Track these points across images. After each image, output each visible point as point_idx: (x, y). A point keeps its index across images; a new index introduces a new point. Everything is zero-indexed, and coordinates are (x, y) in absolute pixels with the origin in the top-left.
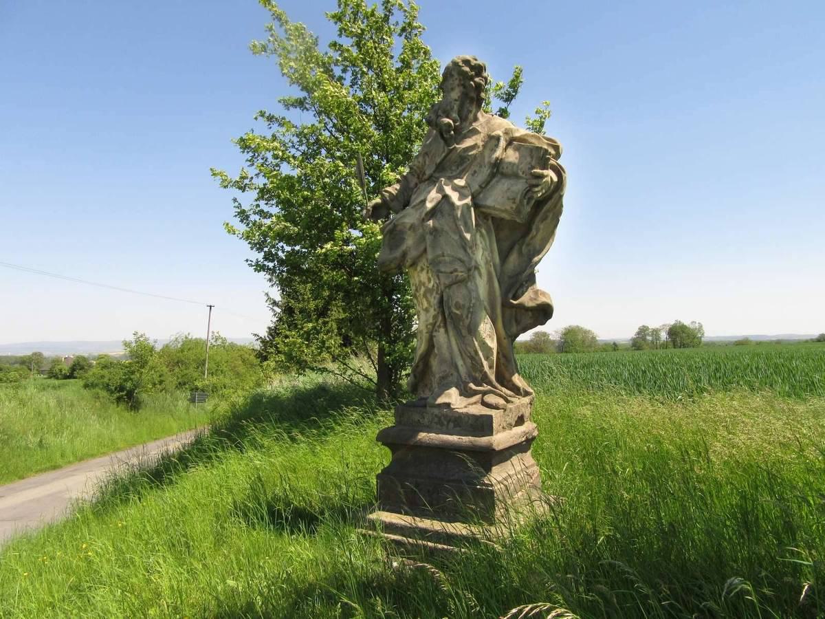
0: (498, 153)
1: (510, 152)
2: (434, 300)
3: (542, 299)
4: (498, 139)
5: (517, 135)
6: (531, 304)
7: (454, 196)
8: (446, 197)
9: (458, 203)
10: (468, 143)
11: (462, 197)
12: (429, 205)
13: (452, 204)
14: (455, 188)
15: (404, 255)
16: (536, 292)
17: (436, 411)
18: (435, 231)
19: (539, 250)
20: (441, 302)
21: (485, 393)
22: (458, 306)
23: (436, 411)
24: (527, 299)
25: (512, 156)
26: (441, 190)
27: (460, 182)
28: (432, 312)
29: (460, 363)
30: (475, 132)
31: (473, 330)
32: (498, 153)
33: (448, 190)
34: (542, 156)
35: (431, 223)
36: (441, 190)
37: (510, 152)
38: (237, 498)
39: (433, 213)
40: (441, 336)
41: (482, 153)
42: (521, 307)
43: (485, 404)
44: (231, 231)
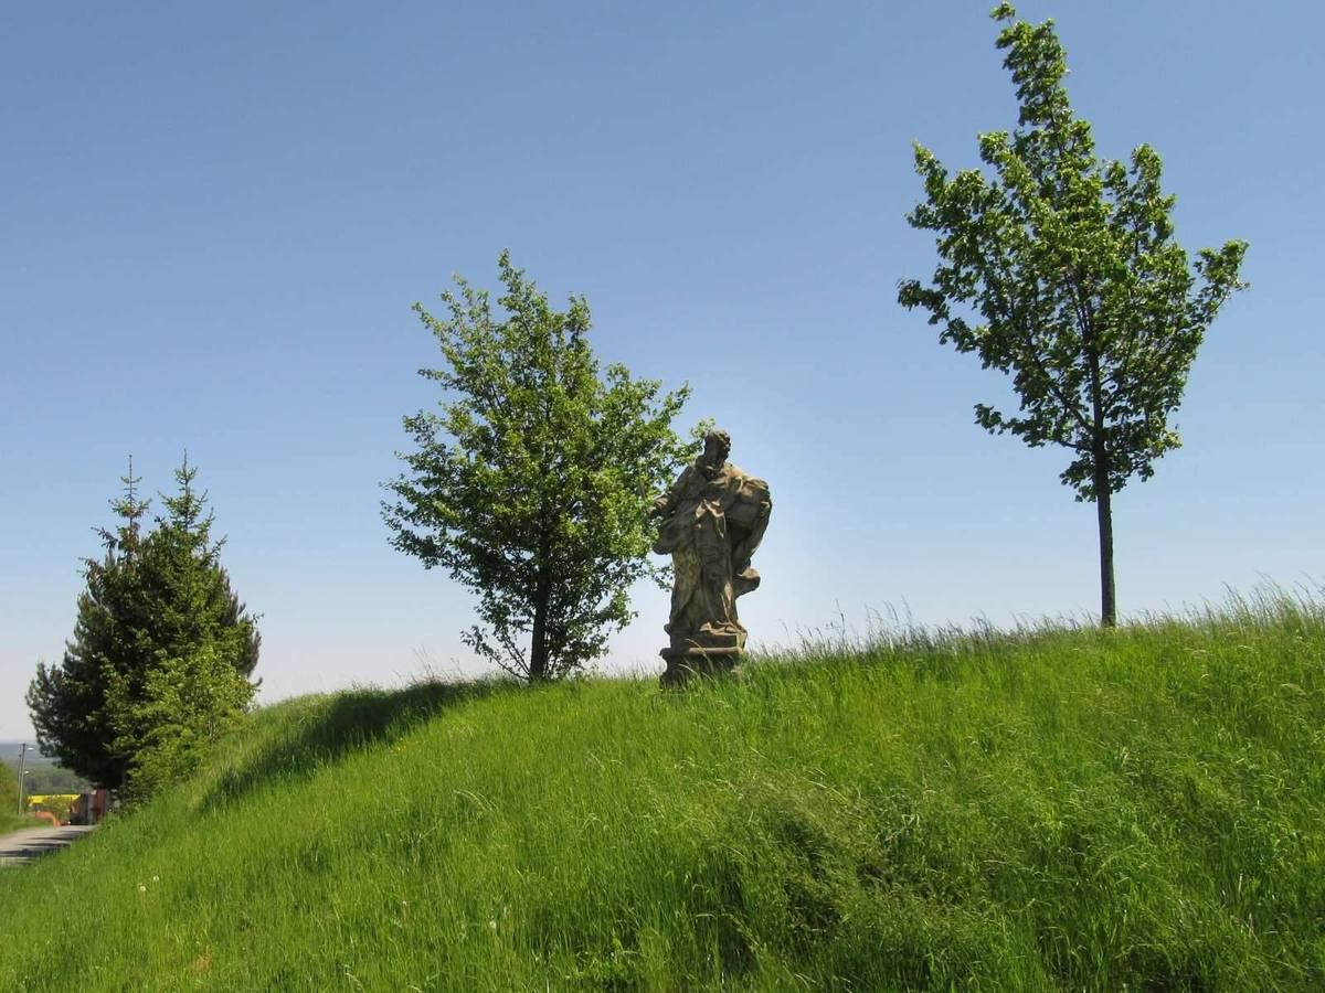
0: (740, 490)
1: (745, 489)
2: (698, 571)
3: (755, 575)
4: (739, 481)
5: (749, 479)
6: (749, 577)
7: (714, 512)
8: (708, 512)
9: (718, 516)
10: (720, 481)
11: (718, 512)
12: (698, 516)
13: (713, 517)
14: (713, 506)
15: (679, 543)
16: (752, 570)
17: (701, 636)
18: (701, 531)
19: (755, 545)
20: (702, 573)
21: (726, 626)
22: (714, 575)
23: (701, 636)
24: (746, 574)
25: (747, 492)
26: (704, 507)
27: (717, 503)
28: (696, 578)
29: (710, 609)
30: (724, 475)
31: (721, 589)
32: (740, 490)
33: (709, 507)
34: (762, 494)
35: (699, 526)
36: (704, 507)
37: (745, 489)
38: (354, 764)
39: (700, 520)
40: (699, 593)
41: (729, 489)
42: (744, 579)
43: (726, 631)
44: (988, 418)
